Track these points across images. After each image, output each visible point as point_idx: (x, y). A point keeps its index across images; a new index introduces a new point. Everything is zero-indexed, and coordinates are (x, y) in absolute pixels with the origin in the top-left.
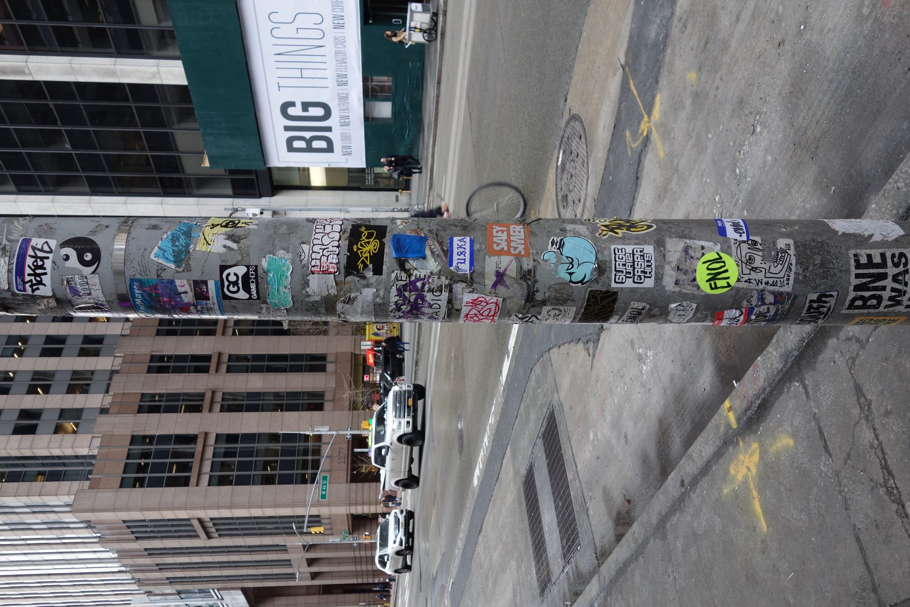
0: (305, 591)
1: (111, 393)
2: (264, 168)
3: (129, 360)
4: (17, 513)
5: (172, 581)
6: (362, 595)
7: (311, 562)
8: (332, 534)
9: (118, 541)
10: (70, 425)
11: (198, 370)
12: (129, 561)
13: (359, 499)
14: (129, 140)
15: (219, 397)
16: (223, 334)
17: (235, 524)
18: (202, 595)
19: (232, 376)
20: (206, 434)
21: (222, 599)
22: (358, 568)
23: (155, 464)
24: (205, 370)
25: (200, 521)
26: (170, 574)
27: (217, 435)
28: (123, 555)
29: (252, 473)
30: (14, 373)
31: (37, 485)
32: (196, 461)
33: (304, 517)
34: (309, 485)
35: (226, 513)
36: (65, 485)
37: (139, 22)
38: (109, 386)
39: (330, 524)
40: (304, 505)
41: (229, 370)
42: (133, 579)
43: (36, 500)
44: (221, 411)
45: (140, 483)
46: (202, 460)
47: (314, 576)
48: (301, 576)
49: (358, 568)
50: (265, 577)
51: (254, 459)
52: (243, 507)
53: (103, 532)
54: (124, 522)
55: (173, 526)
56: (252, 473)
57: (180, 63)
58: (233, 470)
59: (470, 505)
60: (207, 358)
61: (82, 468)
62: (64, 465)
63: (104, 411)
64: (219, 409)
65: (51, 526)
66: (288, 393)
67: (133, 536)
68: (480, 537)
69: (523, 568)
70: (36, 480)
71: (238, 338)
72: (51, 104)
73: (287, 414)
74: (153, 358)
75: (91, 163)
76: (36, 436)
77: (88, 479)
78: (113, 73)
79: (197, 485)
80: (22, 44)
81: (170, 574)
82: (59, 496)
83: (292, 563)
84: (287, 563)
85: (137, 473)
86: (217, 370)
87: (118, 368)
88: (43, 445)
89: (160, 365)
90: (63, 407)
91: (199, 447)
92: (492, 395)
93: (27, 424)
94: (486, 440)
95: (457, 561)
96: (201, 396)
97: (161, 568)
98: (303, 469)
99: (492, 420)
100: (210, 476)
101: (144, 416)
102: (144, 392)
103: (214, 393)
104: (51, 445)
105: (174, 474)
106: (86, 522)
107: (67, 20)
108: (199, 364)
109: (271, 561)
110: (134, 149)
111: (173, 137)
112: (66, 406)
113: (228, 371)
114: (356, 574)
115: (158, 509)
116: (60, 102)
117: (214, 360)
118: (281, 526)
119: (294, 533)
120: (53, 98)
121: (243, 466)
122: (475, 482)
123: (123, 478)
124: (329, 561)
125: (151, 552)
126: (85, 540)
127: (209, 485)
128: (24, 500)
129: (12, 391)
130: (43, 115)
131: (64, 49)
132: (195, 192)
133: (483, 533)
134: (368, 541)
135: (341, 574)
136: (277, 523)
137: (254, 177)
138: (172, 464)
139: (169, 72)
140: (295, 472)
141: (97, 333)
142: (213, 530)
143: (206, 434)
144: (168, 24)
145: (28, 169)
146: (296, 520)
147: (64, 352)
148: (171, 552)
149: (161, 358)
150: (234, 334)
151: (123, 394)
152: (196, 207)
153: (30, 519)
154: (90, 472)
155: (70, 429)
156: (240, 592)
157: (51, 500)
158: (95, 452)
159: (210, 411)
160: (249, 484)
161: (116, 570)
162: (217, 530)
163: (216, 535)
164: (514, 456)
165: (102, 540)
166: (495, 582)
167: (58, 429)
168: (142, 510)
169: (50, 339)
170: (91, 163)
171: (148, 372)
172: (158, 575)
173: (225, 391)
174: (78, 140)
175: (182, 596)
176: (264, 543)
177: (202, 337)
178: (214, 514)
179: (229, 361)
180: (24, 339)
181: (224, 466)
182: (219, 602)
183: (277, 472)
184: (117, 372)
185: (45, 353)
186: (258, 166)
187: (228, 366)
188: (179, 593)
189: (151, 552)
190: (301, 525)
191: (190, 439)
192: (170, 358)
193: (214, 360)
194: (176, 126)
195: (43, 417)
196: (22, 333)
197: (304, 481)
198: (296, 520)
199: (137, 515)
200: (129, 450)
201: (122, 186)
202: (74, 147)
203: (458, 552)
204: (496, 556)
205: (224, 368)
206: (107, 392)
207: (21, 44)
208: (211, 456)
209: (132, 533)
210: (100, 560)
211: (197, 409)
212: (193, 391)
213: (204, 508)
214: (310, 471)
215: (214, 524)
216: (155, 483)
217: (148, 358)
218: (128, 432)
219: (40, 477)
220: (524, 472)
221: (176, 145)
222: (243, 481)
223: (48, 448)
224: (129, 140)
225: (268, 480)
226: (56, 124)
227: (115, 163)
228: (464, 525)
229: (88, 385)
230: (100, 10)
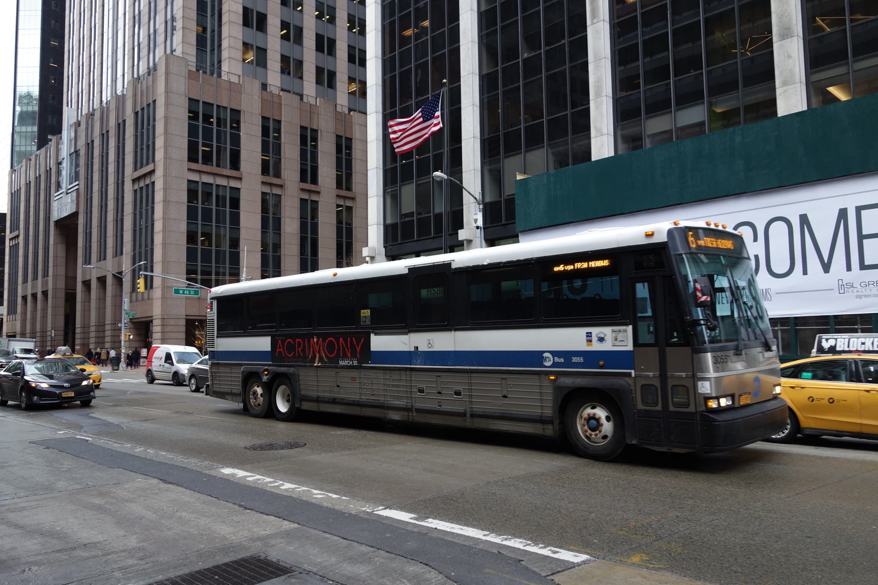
0: (71, 275)
1: (281, 93)
2: (517, 230)
3: (312, 110)
4: (166, 8)
5: (90, 146)
6: (62, 333)
7: (102, 280)
8: (131, 302)
9: (135, 96)
10: (251, 57)
11: (303, 172)
12: (113, 106)
13: (168, 329)
14: (534, 111)
16: (338, 196)
17: (147, 205)
18: (73, 174)
19: (297, 204)
20: (240, 179)
21: (67, 194)
22: (93, 329)
23: (211, 132)
24: (303, 179)
25: (152, 172)
26: (43, 178)
27: (239, 189)
28: (120, 100)
29: (200, 222)
30: (301, 11)
31: (193, 26)
32: (214, 169)
33: (152, 271)
34: (185, 276)
35: (159, 196)
36: (193, 50)
37: (647, 118)
38: (289, 91)
39: (143, 299)
40: (165, 270)
41: (303, 201)
42: (94, 110)
43: (179, 24)
44: (263, 193)
45: (193, 115)
46: (214, 175)
47: (87, 284)
48: (89, 270)
49: (93, 329)
51: (214, 224)
52: (164, 213)
53: (145, 82)
54: (154, 101)
55: (148, 146)
56: (200, 222)
57: (805, 108)
58: (203, 203)
59: (193, 463)
60: (314, 181)
61: (208, 64)
62: (212, 50)
63: (264, 86)
64: (265, 191)
65: (152, 38)
66: (280, 256)
67: (139, 109)
68: (155, 481)
69: (130, 562)
70: (198, 25)
71: (335, 209)
72: (565, 41)
74: (315, 132)
75: (511, 75)
76: (241, 27)
77: (198, 70)
78: (598, 95)
79: (189, 169)
80: (618, 17)
81: (43, 178)
82: (183, 44)
83: (102, 262)
84: (102, 257)
85: (203, 114)
86: (302, 190)
87: (305, 100)
88: (232, 33)
89: (308, 138)
90: (268, 51)
91: (228, 172)
92: (352, 495)
93: (254, 20)
94: (287, 486)
95: (116, 446)
96: (278, 175)
97: (104, 136)
98: (202, 271)
99: (318, 494)
100: (197, 182)
101: (259, 122)
102: (283, 123)
103: (281, 186)
104: (232, 39)
105: (201, 148)
106: (155, 69)
107: (644, 56)
108: (309, 173)
109: (105, 241)
110: (525, 113)
111: (698, 104)
113: (301, 199)
114: (86, 327)
115: (166, 132)
116: (567, 49)
117: (313, 187)
118: (143, 251)
119: (134, 263)
120: (570, 43)
121: (207, 214)
122: (227, 471)
123: (198, 101)
124: (102, 299)
125: (121, 127)
126: (136, 68)
128: (179, 14)
129: (284, 8)
130: (554, 33)
131: (617, 52)
132: (486, 168)
133: (163, 485)
134: (123, 338)
135: (86, 311)
136: (146, 246)
137: (503, 222)
138: (211, 146)
139: (602, 144)
140: (199, 264)
141: (338, 84)
142: (142, 184)
143: (240, 179)
144: (648, 144)
145: (502, 21)
146: (149, 265)
147: (320, 54)
148: (121, 145)
149: (315, 139)
150: (338, 206)
151: (281, 104)
152: (472, 168)
153: (160, 19)
154: (205, 72)
155: (246, 57)
156: (74, 210)
157: (178, 37)
158: (224, 77)
159: (263, 183)
161: (104, 99)
163: (136, 187)
164: (288, 534)
165: (136, 81)
166: (99, 509)
167: (246, 46)
168: (166, 118)
169: (332, 43)
170: (511, 75)
171: (301, 127)
173: (283, 197)
174: (532, 66)
175: (74, 155)
176: (125, 234)
177: (335, 176)
178: (159, 185)
180: (332, 20)
181: (207, 195)
183: (200, 247)
184: (302, 99)
185: (319, 38)
186: (519, 226)
187: (307, 200)
188: (76, 152)
189: (121, 127)
190: (149, 269)
191: (235, 163)
192: (315, 147)
193: (313, 187)
194: (550, 151)
195: (259, 34)
196: (337, 19)
197: (189, 272)
198: (149, 265)
199: (160, 113)
200: (226, 108)
201: (488, 102)
202: (525, 61)
203: (127, 447)
204: (136, 509)
205: (305, 196)
206: (282, 90)
207: (618, 17)
208: (218, 183)
209: (143, 109)
210: (114, 80)
211: (265, 170)
212: (283, 167)
213: (165, 176)
214: (199, 277)
216: (192, 131)
217: (315, 127)
218: (243, 107)
219: (201, 29)
220: (274, 555)
221: (509, 156)
222: (192, 213)
223: (230, 36)
224: (534, 111)
225: (191, 237)
226: (547, 44)
227: (512, 96)
228: (164, 456)
229: (289, 74)
230: (629, 93)
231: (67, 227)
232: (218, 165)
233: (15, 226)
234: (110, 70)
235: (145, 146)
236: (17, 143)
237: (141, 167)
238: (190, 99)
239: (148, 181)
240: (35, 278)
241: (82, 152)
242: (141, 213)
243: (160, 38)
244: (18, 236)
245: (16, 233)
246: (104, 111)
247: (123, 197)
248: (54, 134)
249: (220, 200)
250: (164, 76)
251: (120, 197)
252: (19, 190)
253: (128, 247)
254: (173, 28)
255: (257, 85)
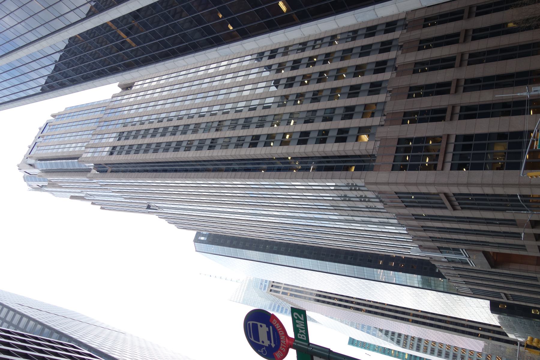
5: (461, 276)
9: (395, 207)
15: (458, 110)
19: (468, 94)
20: (448, 136)
23: (411, 155)
25: (446, 195)
41: (465, 90)
43: (350, 181)
45: (403, 168)
50: (500, 245)
54: (396, 193)
60: (449, 84)
62: (363, 161)
64: (458, 118)
65: (362, 199)
67: (403, 205)
73: (514, 118)
76: (347, 143)
79: (442, 169)
81: (461, 273)
89: (415, 91)
90: (360, 126)
97: (426, 229)
108: (442, 89)
112: (362, 125)
113: (464, 92)
117: (453, 85)
125: (418, 217)
127: (451, 170)
142: (456, 203)
157: (360, 183)
159: (451, 119)
160: (482, 170)
161: (405, 232)
162: (460, 204)
163: (459, 207)
172: (455, 272)
178: (455, 190)
179: (465, 84)
181: (462, 157)
182: (467, 259)
189: (418, 217)
193: (453, 85)
209: (403, 202)
215: (457, 199)
231: (495, 261)
232: (439, 151)
233: (498, 295)
234: (386, 227)
235: (428, 201)
236: (442, 289)
237: (443, 203)
238: (392, 170)
239: (454, 199)
240: (517, 236)
241: (439, 245)
242: (479, 204)
243: (370, 204)
244: (505, 294)
245: (503, 295)
246: (410, 229)
247: (468, 218)
248: (435, 270)
249: (466, 148)
250: (379, 186)
251: (468, 220)
252: (471, 289)
253: (508, 215)
254: (361, 197)
255: (380, 129)
